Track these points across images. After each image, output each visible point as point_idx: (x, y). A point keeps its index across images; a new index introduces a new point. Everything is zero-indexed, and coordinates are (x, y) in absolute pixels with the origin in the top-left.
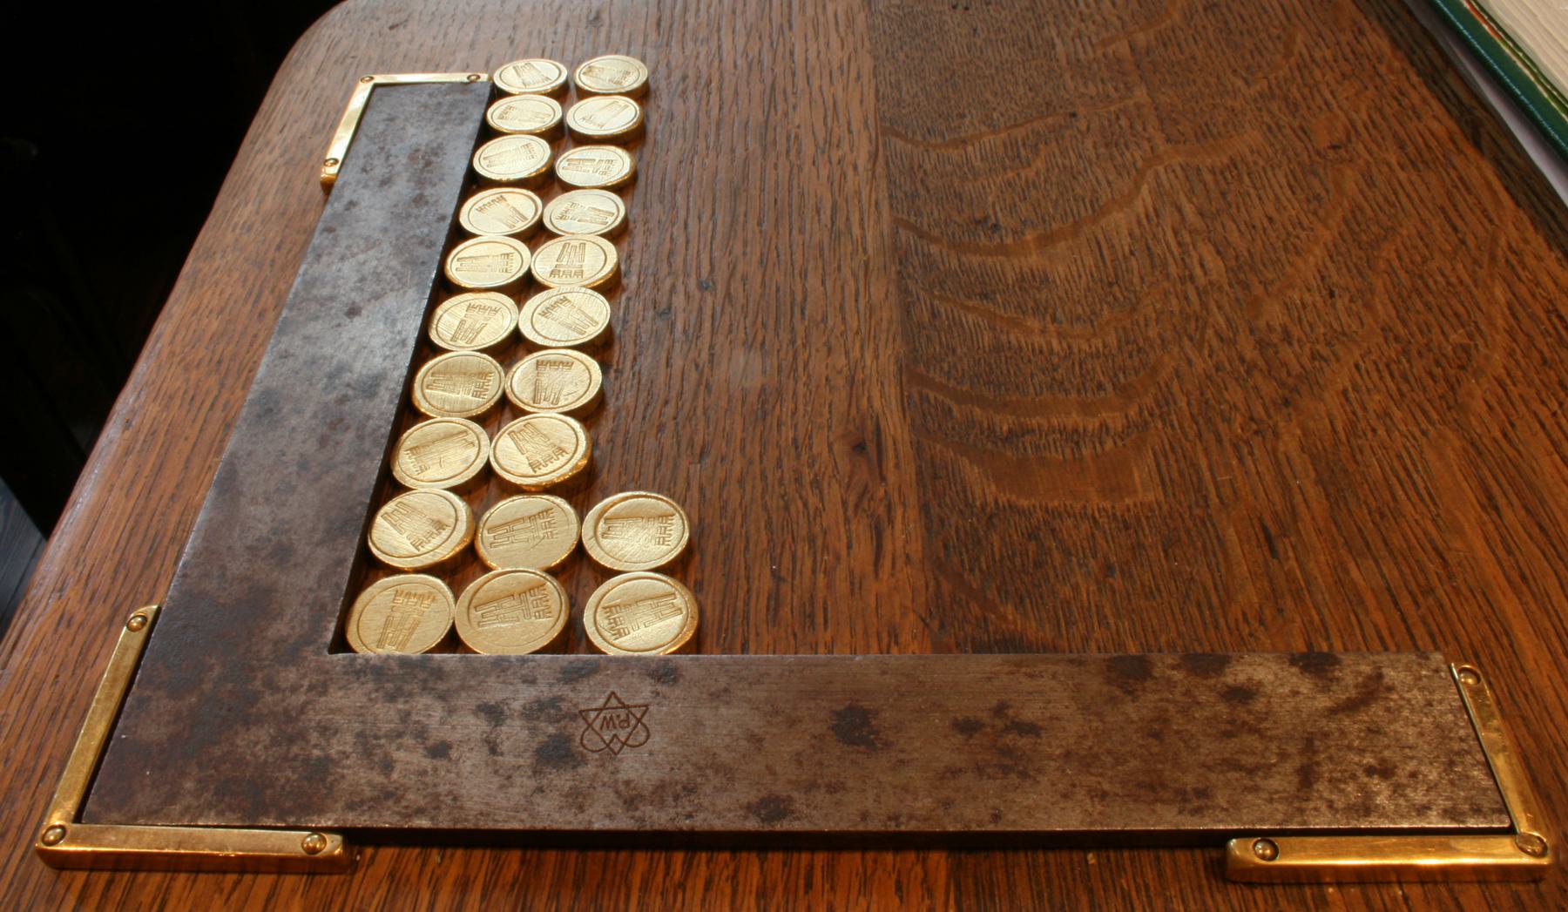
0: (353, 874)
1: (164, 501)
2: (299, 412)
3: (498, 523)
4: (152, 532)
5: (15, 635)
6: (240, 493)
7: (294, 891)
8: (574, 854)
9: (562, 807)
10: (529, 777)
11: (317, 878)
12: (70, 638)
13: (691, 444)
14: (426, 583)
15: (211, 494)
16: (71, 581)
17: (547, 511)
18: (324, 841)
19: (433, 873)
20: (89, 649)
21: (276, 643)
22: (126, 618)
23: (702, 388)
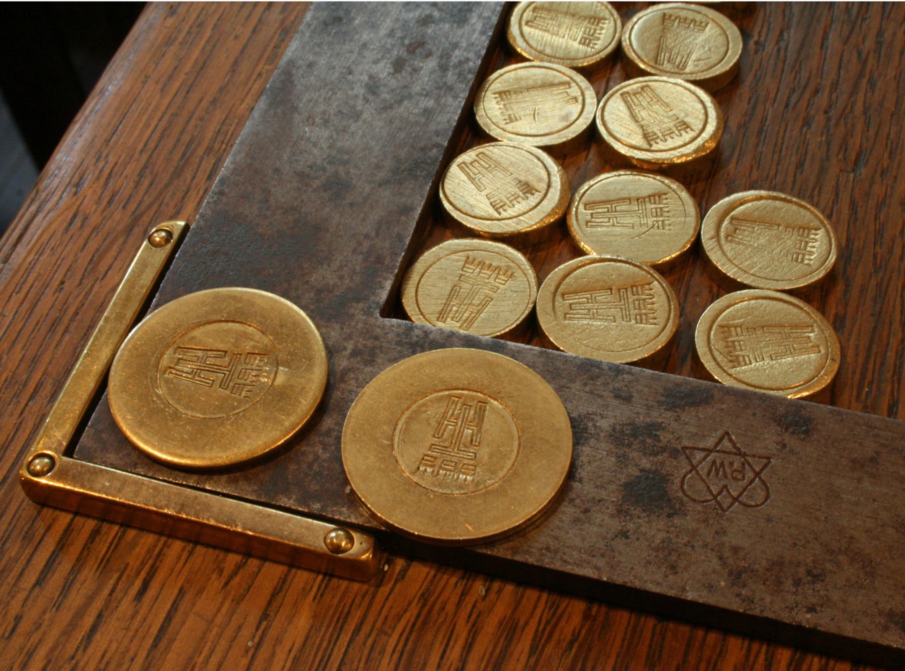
0: (379, 585)
1: (204, 103)
2: (374, 27)
3: (598, 199)
4: (186, 138)
5: (21, 226)
6: (295, 109)
7: (305, 591)
8: (651, 622)
9: (649, 562)
10: (612, 516)
11: (335, 581)
12: (81, 242)
13: (844, 145)
14: (504, 255)
15: (262, 104)
16: (89, 178)
17: (660, 195)
18: (351, 540)
19: (474, 607)
20: (101, 258)
21: (319, 292)
22: (146, 231)
23: (864, 81)
